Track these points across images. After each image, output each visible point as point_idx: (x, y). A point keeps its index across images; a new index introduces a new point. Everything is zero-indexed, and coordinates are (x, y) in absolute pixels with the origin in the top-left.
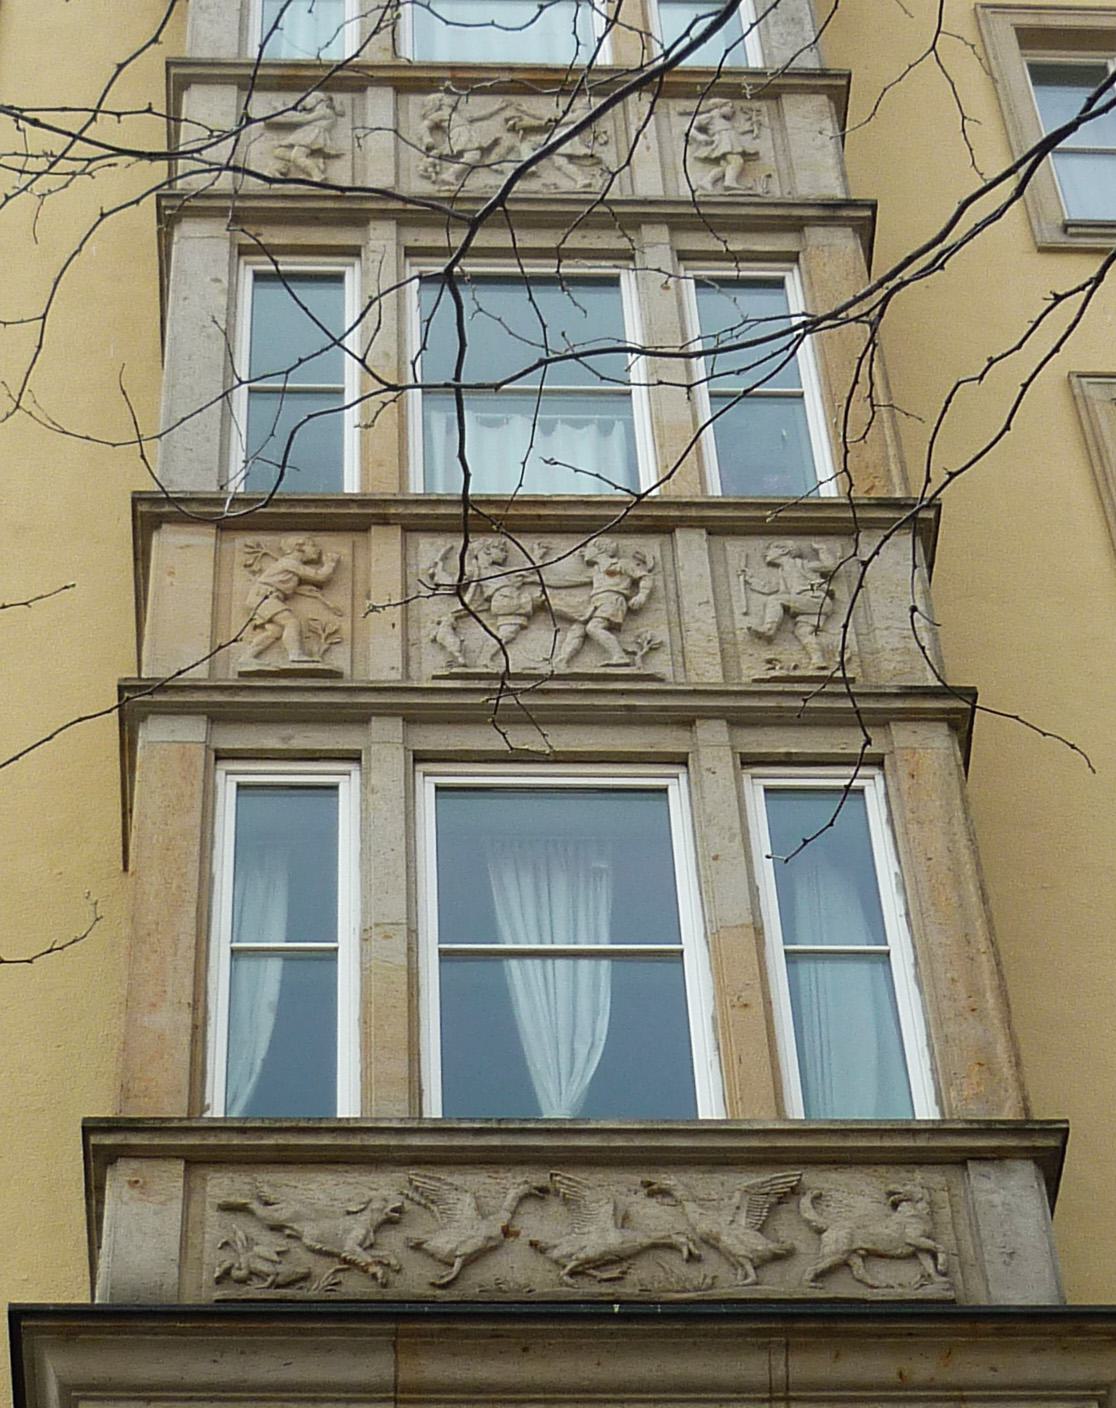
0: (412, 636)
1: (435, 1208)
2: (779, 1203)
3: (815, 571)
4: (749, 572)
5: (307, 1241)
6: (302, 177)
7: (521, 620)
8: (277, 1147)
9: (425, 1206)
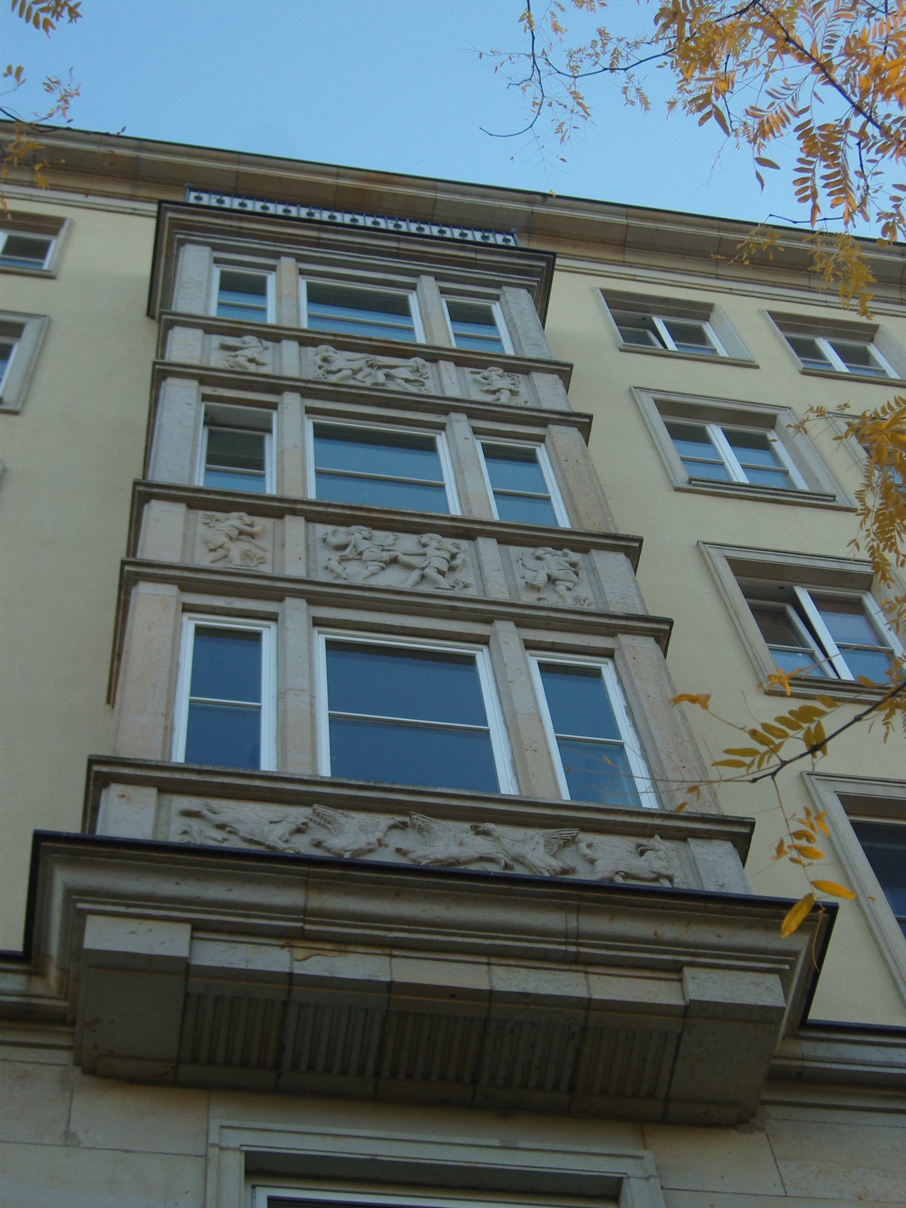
0: (312, 565)
1: (329, 826)
2: (564, 846)
3: (566, 562)
4: (524, 559)
5: (242, 834)
6: (242, 370)
7: (383, 565)
8: (222, 785)
9: (324, 826)
